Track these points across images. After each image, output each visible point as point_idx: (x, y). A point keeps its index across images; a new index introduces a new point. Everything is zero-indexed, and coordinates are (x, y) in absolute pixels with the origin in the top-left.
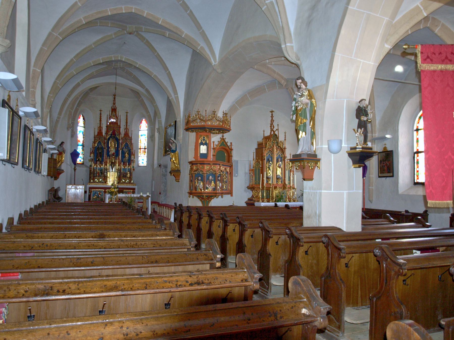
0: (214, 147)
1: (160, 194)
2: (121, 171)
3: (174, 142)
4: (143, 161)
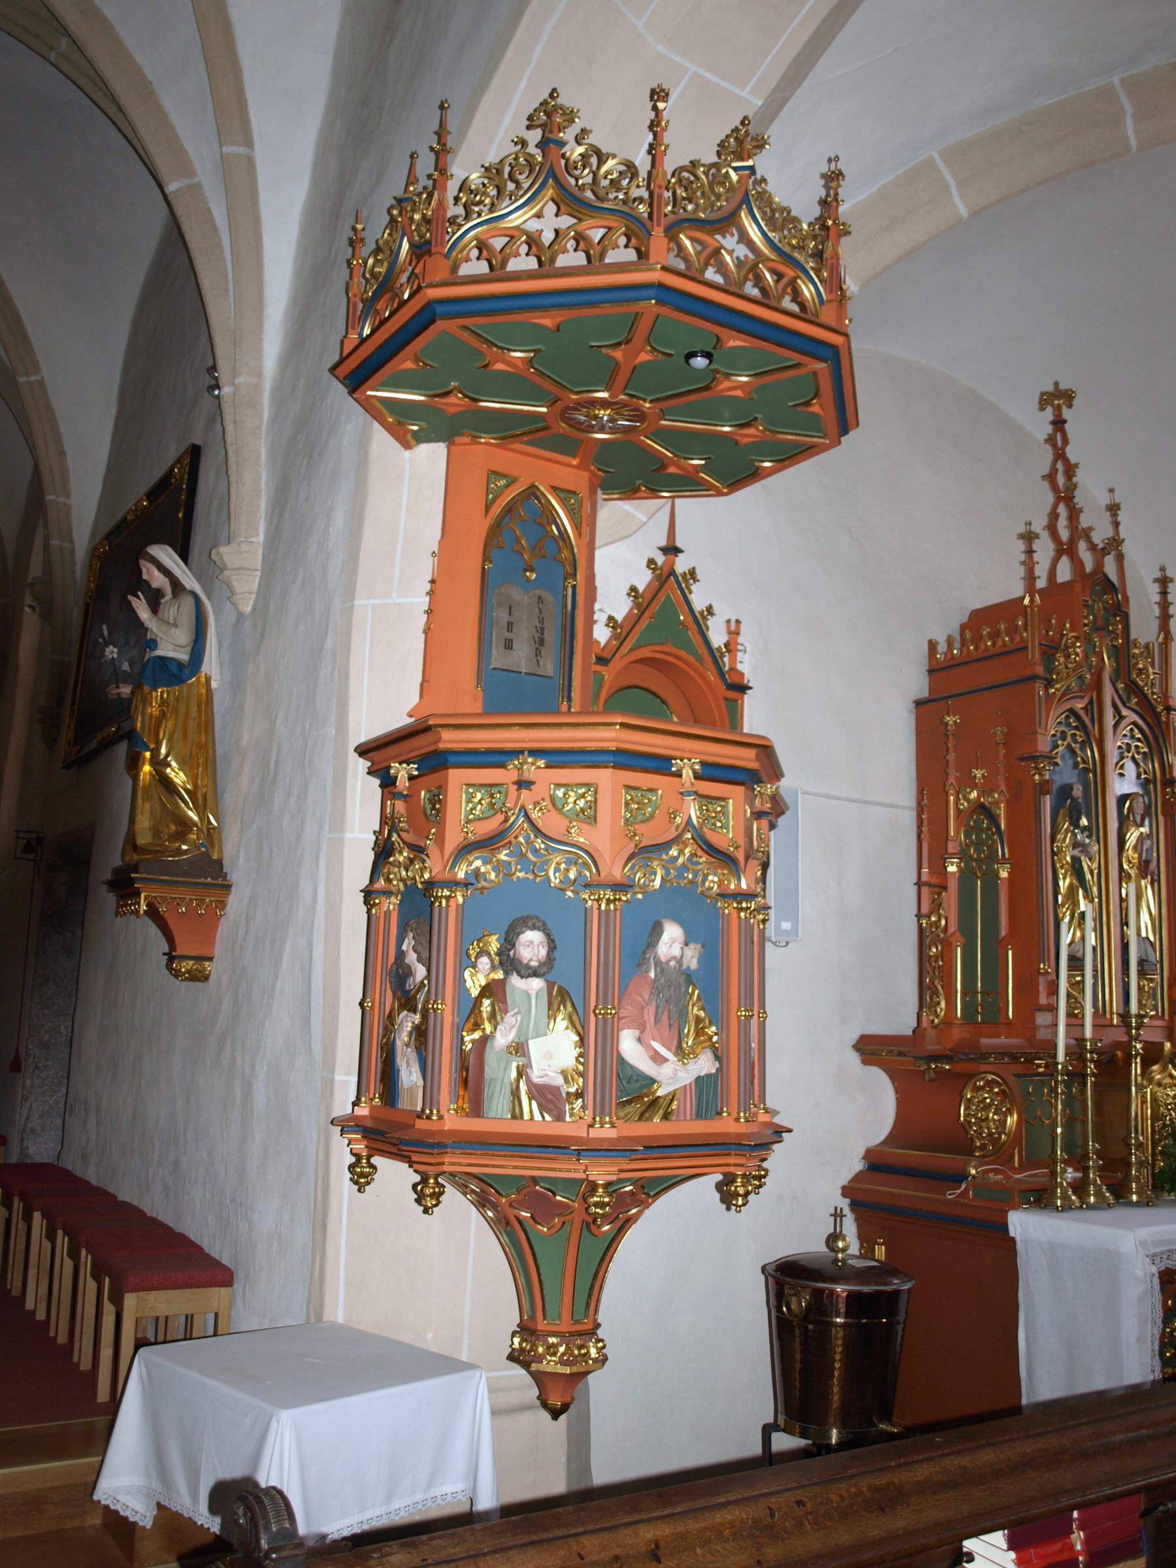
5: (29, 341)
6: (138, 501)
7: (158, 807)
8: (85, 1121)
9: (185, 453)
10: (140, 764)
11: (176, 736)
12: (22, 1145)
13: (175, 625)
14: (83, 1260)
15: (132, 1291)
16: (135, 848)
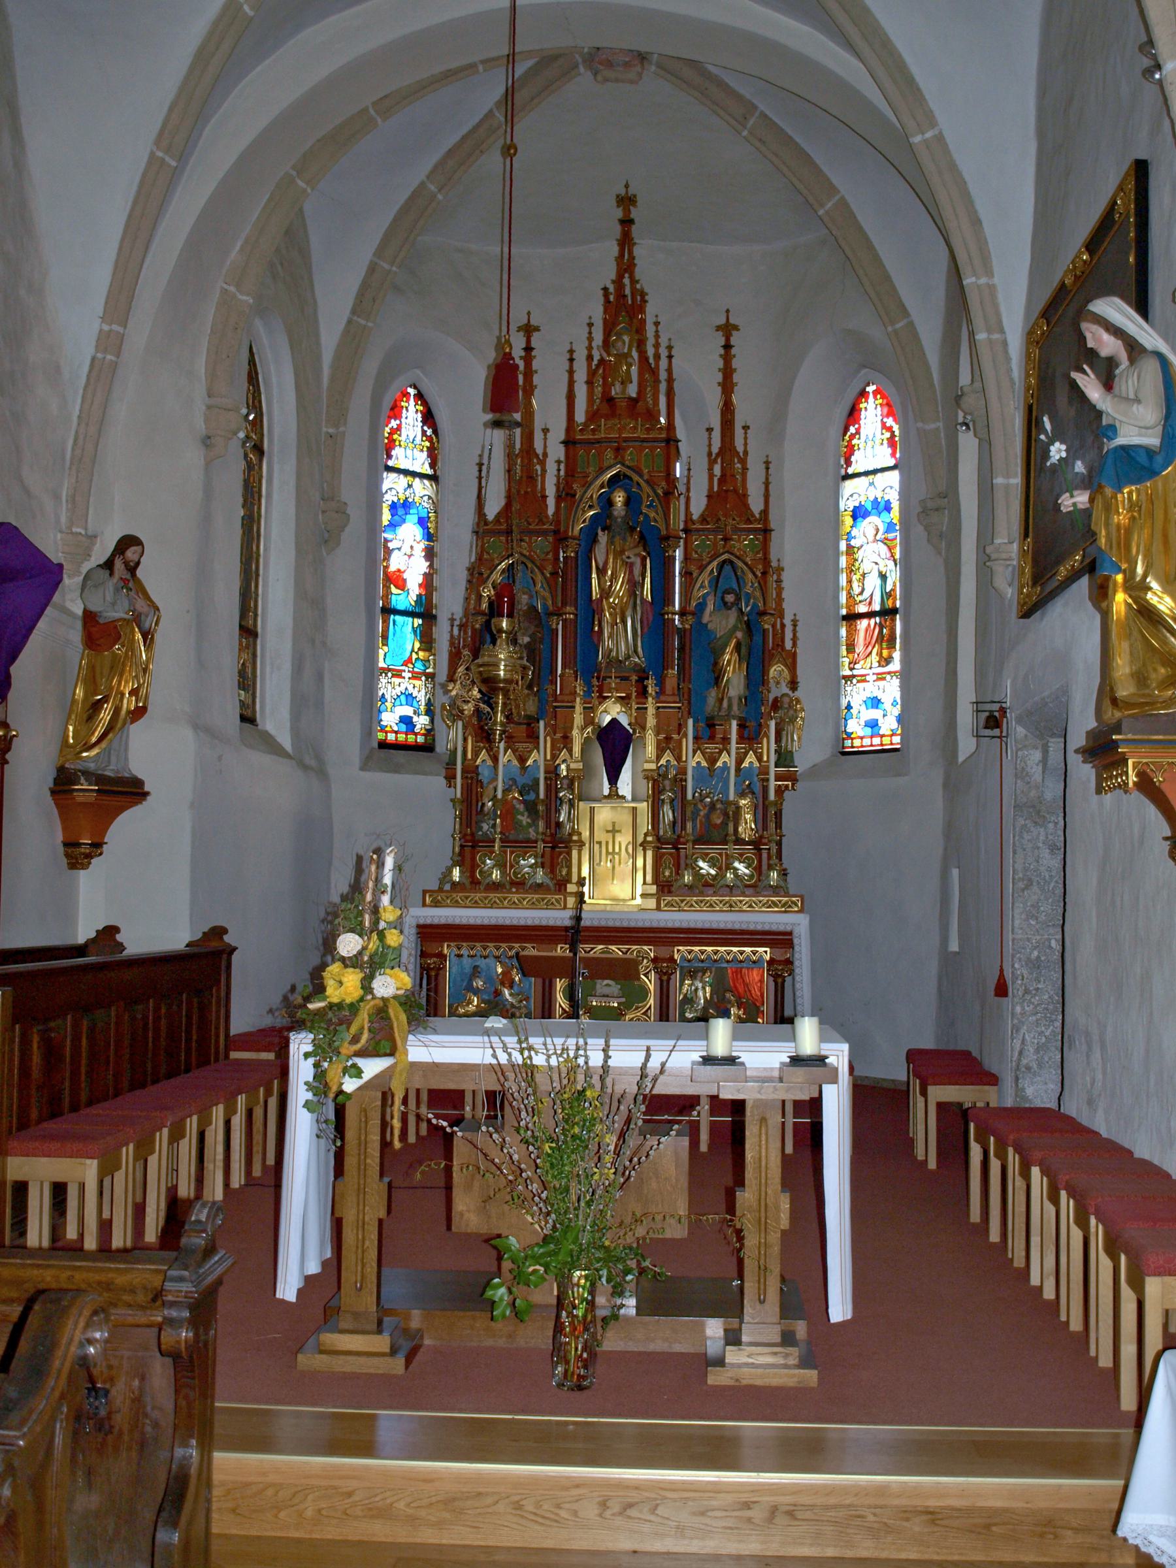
1: (1002, 990)
2: (684, 789)
3: (1134, 348)
4: (875, 714)
5: (919, 89)
6: (1076, 257)
7: (1139, 645)
8: (1088, 1056)
9: (1127, 174)
10: (1110, 592)
11: (1154, 549)
12: (1017, 1085)
13: (1137, 401)
14: (1093, 1230)
15: (1155, 1275)
16: (1114, 701)
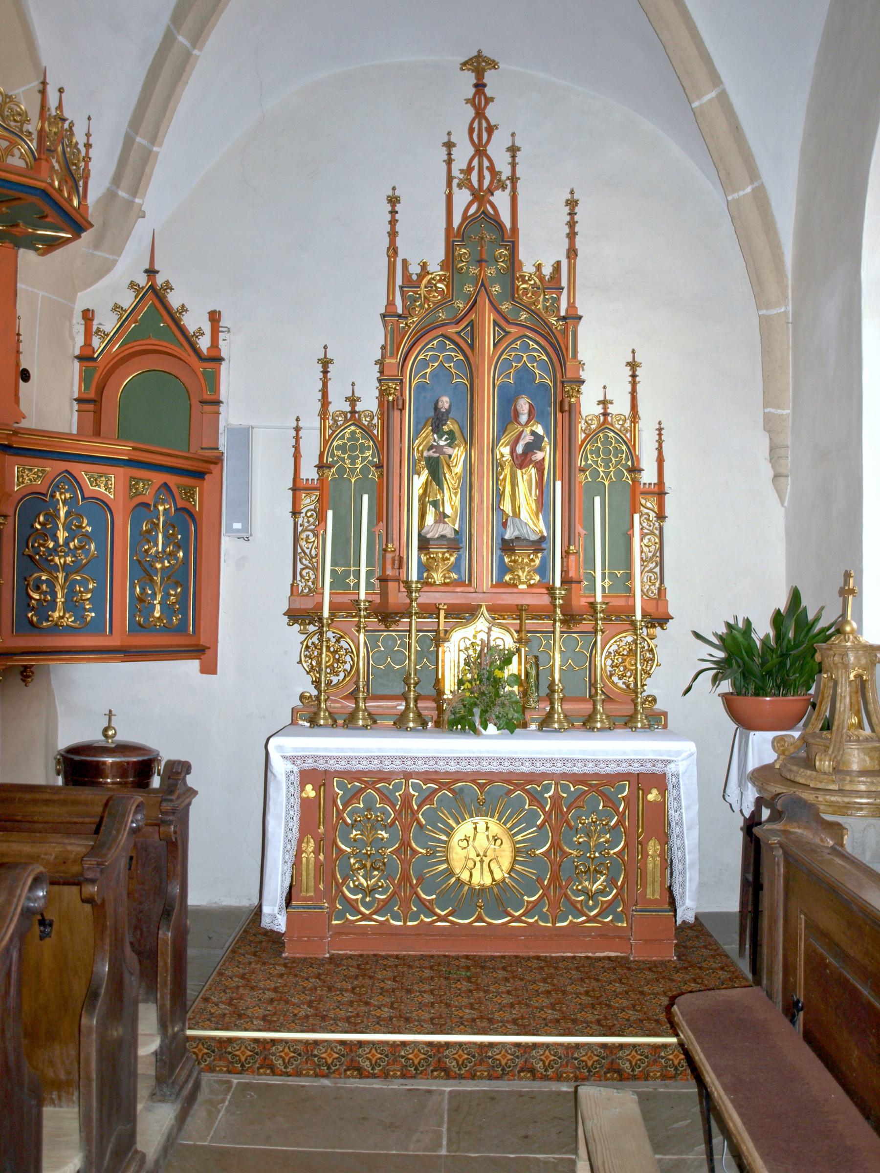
0: (88, 344)
